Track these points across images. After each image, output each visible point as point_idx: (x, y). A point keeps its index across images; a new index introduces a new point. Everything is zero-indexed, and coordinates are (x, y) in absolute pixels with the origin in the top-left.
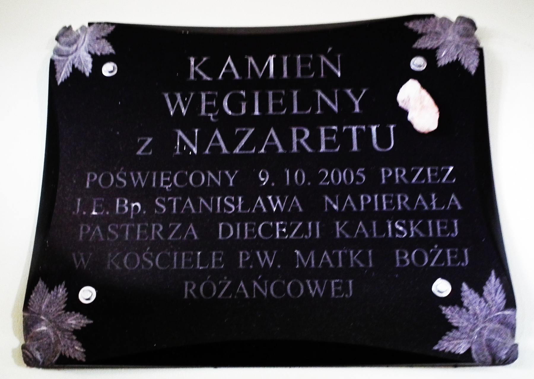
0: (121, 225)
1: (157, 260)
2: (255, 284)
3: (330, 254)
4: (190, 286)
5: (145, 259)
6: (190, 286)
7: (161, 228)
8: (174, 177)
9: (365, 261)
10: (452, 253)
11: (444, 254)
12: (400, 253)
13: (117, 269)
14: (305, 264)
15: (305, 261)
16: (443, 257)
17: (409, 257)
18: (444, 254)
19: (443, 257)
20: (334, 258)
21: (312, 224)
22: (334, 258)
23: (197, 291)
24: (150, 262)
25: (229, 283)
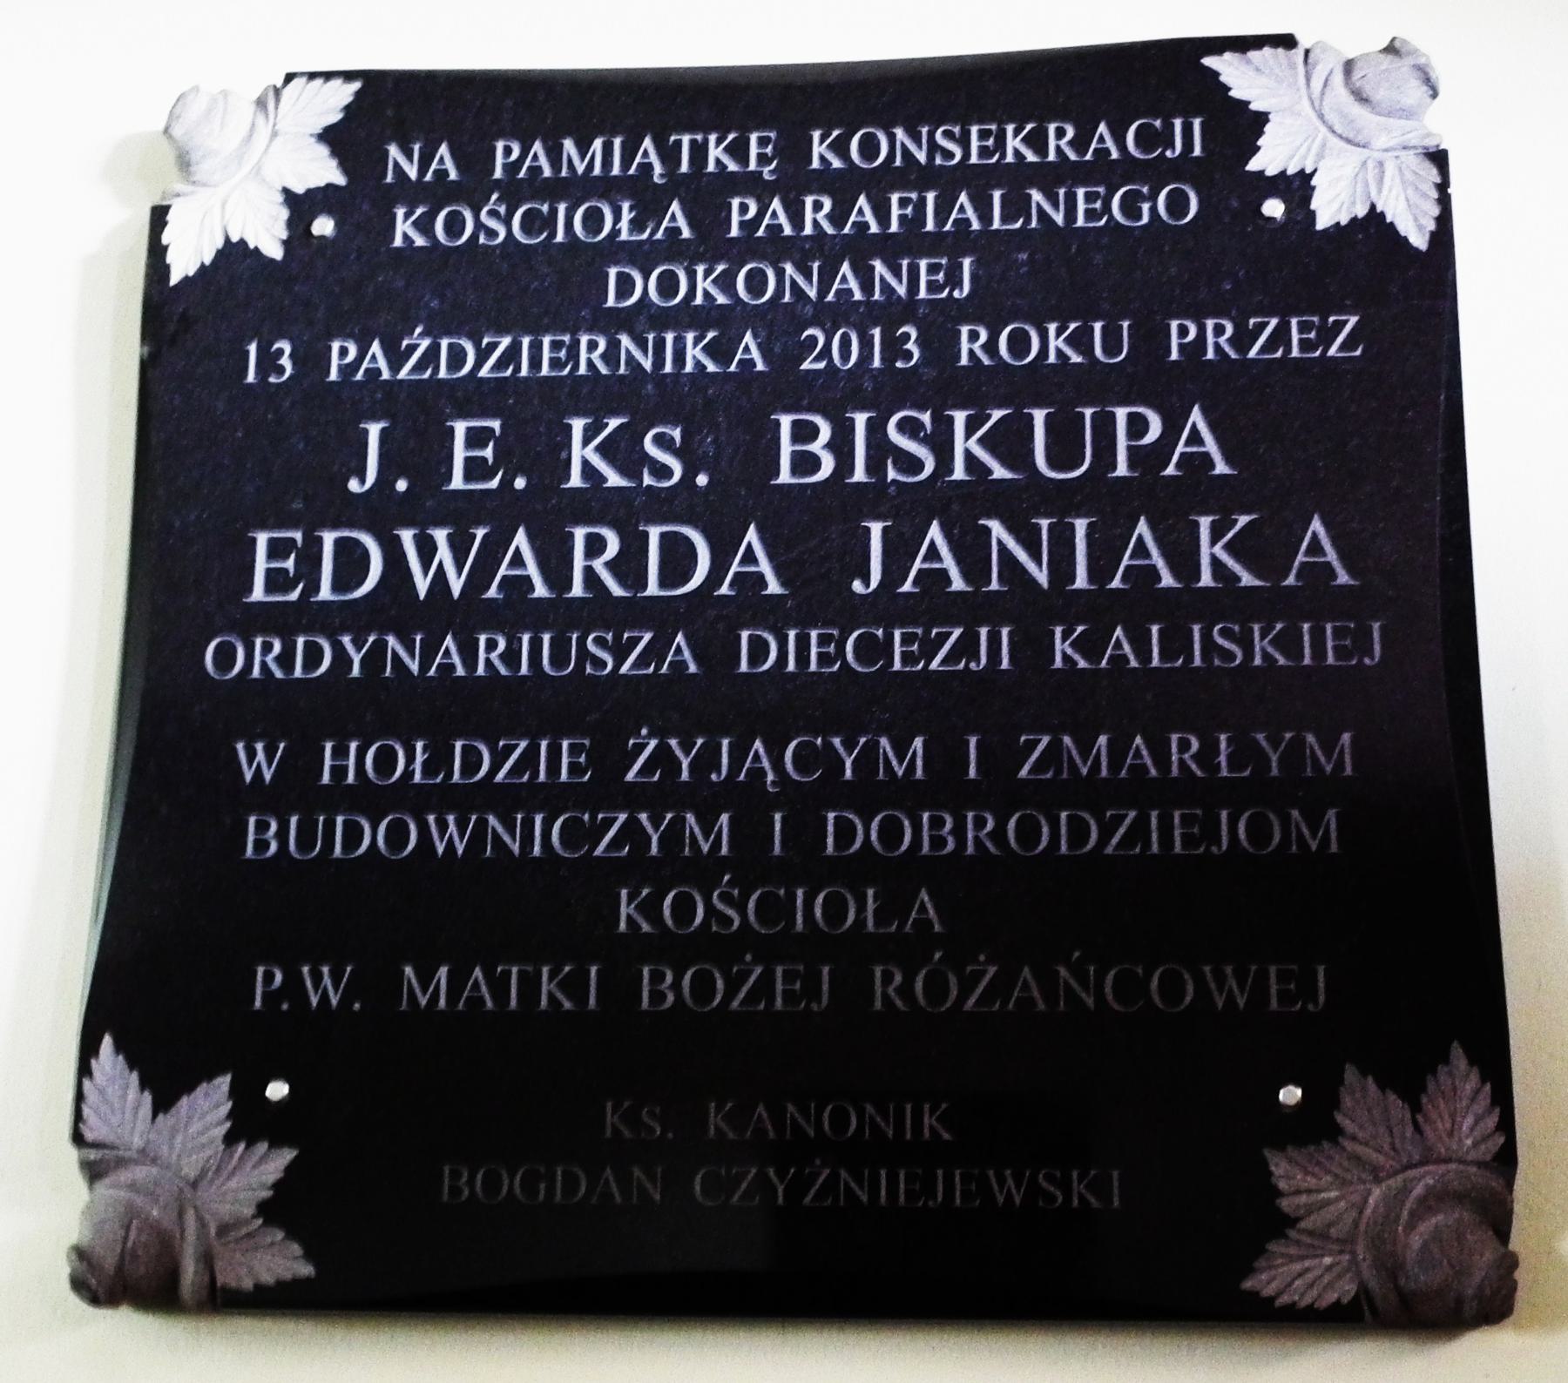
0: (772, 793)
1: (751, 905)
2: (1063, 972)
3: (489, 974)
4: (887, 978)
5: (720, 906)
6: (887, 978)
7: (1195, 745)
8: (487, 770)
9: (580, 996)
10: (789, 977)
11: (767, 981)
12: (652, 973)
13: (644, 930)
14: (423, 1001)
15: (424, 993)
16: (765, 986)
17: (676, 985)
18: (767, 981)
19: (765, 986)
20: (499, 987)
21: (1160, 818)
22: (499, 987)
23: (906, 991)
24: (731, 912)
25: (992, 970)
